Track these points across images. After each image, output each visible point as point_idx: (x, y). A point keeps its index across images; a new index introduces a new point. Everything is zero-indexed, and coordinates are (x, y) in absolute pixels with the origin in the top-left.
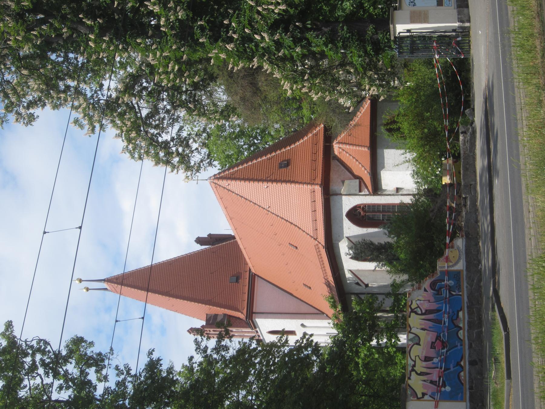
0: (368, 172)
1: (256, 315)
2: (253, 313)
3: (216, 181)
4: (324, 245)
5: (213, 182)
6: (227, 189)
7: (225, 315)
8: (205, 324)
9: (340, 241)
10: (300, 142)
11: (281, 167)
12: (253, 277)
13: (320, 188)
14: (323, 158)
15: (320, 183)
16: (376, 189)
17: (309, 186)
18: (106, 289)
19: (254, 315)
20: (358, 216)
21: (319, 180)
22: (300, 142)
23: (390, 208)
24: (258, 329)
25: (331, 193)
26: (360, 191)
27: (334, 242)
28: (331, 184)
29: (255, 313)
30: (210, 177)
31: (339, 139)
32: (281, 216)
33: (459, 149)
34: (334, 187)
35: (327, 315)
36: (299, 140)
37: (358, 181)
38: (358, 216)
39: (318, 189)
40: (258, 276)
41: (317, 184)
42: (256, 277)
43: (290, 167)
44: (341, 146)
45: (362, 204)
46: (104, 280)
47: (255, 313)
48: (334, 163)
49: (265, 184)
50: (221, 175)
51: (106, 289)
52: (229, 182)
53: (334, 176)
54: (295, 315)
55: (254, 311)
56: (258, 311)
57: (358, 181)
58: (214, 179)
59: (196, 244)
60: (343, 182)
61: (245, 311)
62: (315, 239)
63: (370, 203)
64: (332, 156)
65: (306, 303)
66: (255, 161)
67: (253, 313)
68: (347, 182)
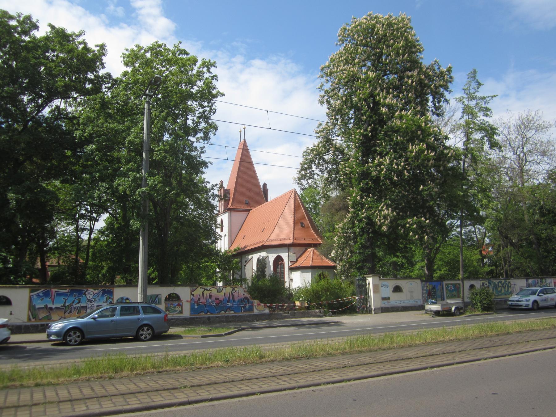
12: (248, 211)
16: (292, 269)
20: (278, 261)
21: (295, 242)
34: (292, 249)
38: (278, 261)
44: (312, 253)
48: (303, 249)
53: (297, 249)
60: (295, 253)
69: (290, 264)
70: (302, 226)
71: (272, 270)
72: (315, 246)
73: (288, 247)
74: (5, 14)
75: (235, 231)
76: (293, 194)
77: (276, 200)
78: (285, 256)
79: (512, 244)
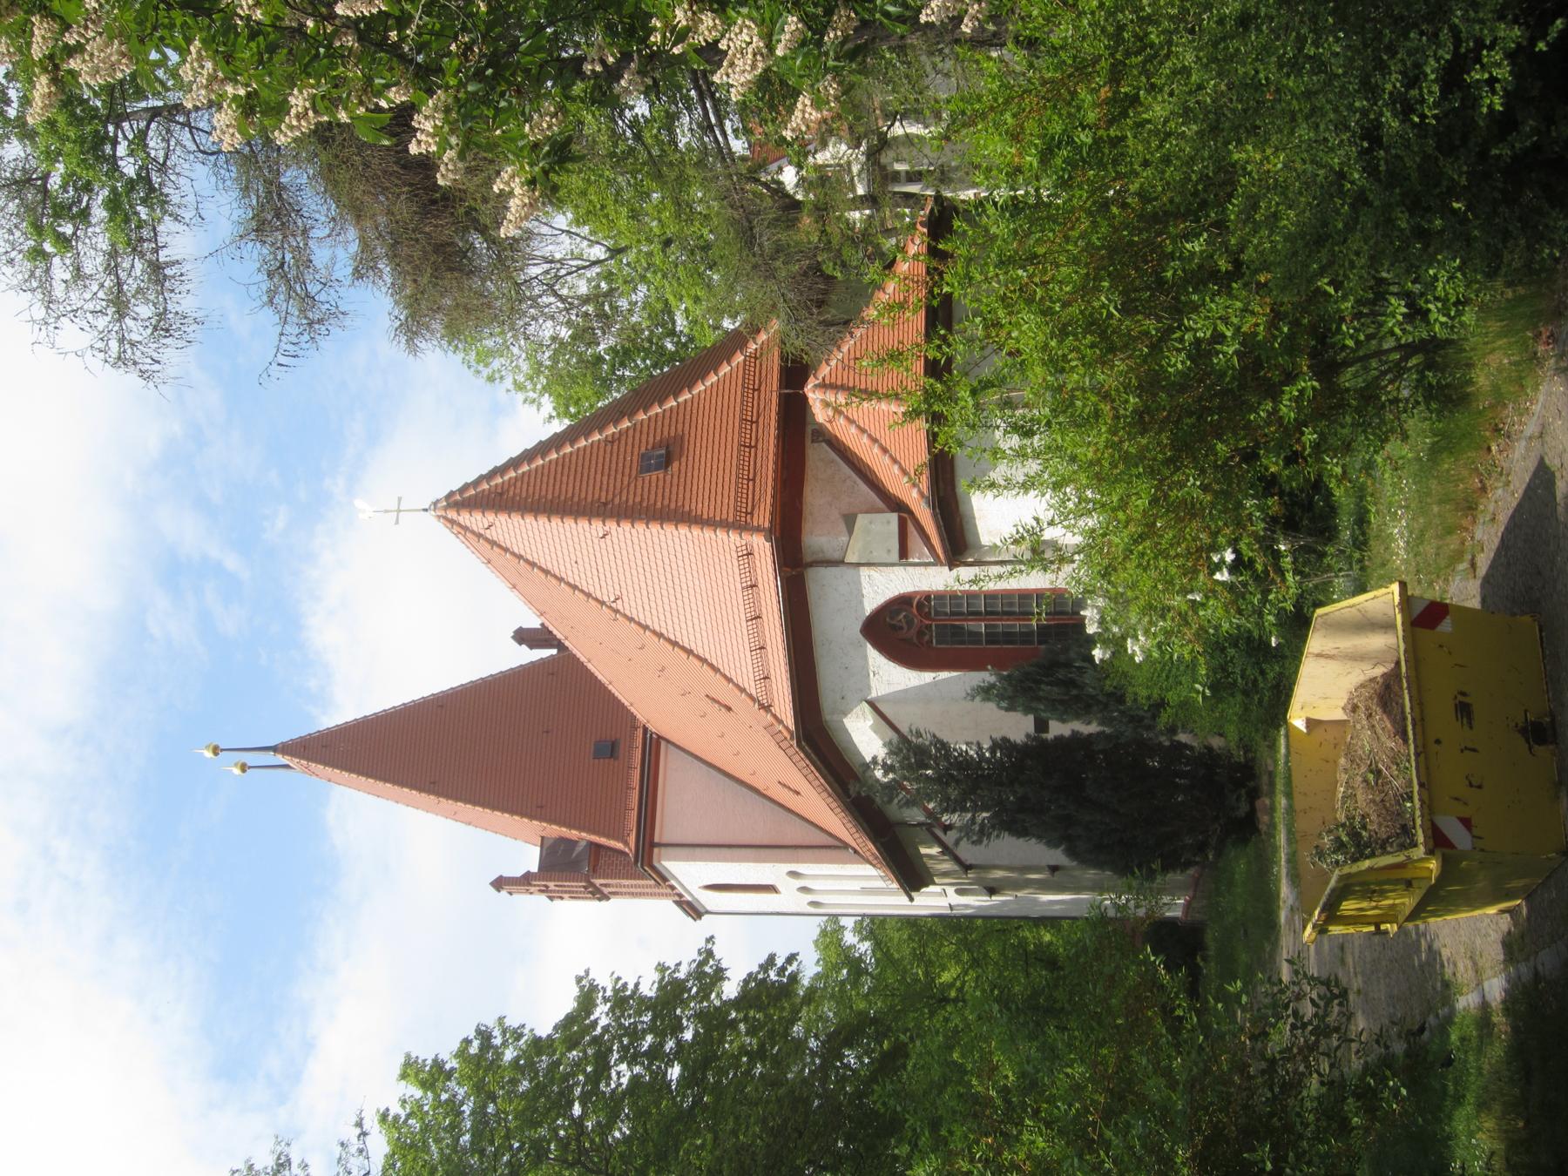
0: (921, 494)
1: (663, 850)
2: (653, 845)
3: (452, 514)
4: (792, 727)
5: (445, 518)
6: (487, 540)
7: (591, 844)
8: (534, 868)
9: (845, 715)
10: (708, 384)
11: (646, 464)
12: (654, 744)
13: (768, 545)
14: (778, 437)
15: (767, 525)
16: (957, 542)
17: (734, 536)
18: (287, 766)
19: (656, 850)
20: (904, 631)
21: (763, 517)
22: (708, 384)
23: (1011, 604)
24: (673, 882)
25: (808, 558)
26: (904, 553)
27: (828, 716)
28: (807, 527)
29: (660, 845)
30: (435, 503)
31: (824, 371)
32: (657, 629)
33: (1334, 601)
34: (818, 537)
35: (856, 851)
36: (703, 377)
37: (894, 517)
38: (904, 631)
39: (763, 548)
40: (668, 741)
41: (758, 529)
42: (663, 744)
43: (676, 464)
44: (830, 396)
45: (916, 593)
46: (274, 749)
47: (660, 845)
48: (816, 455)
49: (598, 526)
50: (466, 495)
51: (287, 766)
52: (490, 517)
53: (816, 498)
54: (768, 851)
55: (656, 840)
56: (665, 840)
57: (894, 517)
58: (445, 508)
59: (515, 644)
60: (850, 521)
61: (632, 839)
62: (766, 708)
63: (941, 588)
64: (809, 430)
65: (798, 815)
66: (641, 416)
67: (653, 845)
68: (862, 520)
69: (919, 551)
70: (667, 462)
71: (955, 674)
72: (795, 373)
73: (795, 566)
74: (406, 1148)
75: (762, 826)
76: (465, 518)
77: (530, 602)
78: (881, 586)
79: (63, 82)
